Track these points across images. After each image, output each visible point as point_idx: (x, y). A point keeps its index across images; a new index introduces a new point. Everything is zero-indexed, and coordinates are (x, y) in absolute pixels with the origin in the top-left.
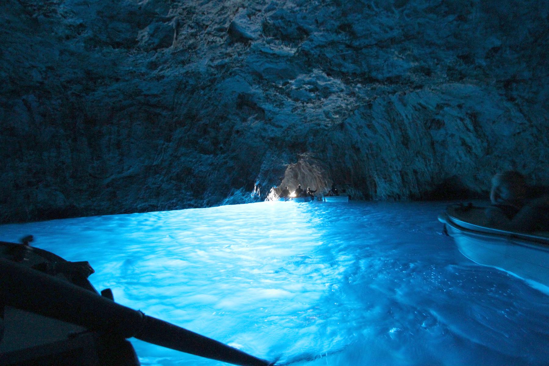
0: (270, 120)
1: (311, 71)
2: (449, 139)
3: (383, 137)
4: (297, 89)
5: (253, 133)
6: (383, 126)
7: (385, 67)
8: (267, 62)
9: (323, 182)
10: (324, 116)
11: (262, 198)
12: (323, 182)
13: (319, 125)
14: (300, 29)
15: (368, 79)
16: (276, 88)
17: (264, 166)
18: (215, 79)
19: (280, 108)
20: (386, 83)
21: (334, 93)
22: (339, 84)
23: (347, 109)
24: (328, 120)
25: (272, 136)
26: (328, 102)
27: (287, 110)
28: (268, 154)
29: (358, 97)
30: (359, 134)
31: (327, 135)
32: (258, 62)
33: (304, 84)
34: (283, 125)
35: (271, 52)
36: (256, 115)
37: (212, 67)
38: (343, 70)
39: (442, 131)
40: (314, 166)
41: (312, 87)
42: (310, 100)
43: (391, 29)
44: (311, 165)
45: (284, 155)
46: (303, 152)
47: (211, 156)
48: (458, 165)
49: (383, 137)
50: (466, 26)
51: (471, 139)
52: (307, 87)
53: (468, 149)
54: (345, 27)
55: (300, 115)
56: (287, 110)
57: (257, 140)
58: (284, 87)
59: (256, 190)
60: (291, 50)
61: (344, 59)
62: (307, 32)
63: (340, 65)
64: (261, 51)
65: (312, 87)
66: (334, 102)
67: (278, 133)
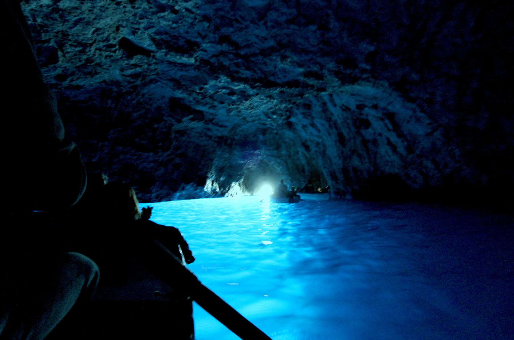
2: (378, 138)
5: (197, 133)
6: (323, 125)
8: (179, 70)
11: (222, 192)
13: (265, 125)
14: (188, 41)
18: (137, 86)
28: (219, 152)
31: (277, 134)
34: (227, 124)
36: (191, 116)
39: (370, 130)
43: (266, 39)
45: (235, 152)
46: (255, 149)
47: (151, 154)
48: (389, 164)
50: (331, 35)
51: (394, 138)
53: (394, 148)
54: (224, 39)
57: (204, 138)
62: (198, 45)
67: (225, 132)
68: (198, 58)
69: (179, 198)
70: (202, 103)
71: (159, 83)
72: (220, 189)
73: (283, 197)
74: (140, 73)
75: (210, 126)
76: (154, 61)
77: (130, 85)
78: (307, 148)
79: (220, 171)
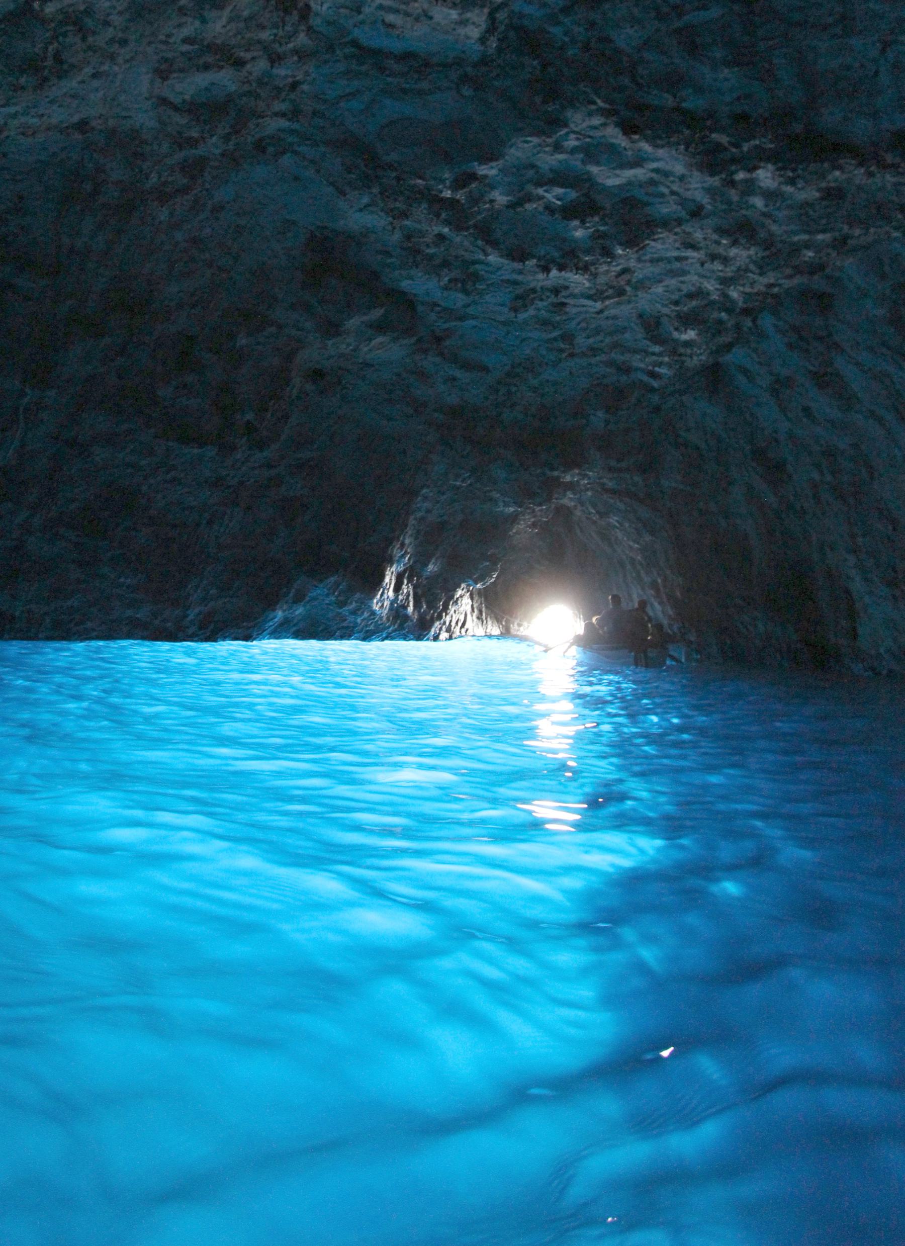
0: (439, 340)
1: (556, 122)
3: (880, 420)
4: (511, 206)
7: (884, 79)
9: (647, 579)
10: (640, 334)
11: (418, 622)
12: (647, 579)
15: (805, 146)
16: (436, 202)
17: (427, 506)
18: (201, 163)
19: (467, 293)
20: (889, 158)
21: (665, 223)
22: (682, 178)
23: (727, 305)
24: (657, 349)
25: (453, 399)
26: (650, 270)
27: (495, 302)
29: (768, 244)
30: (783, 410)
31: (657, 409)
32: (352, 95)
33: (539, 184)
35: (397, 46)
36: (377, 313)
37: (176, 109)
38: (693, 103)
40: (613, 520)
41: (573, 194)
42: (569, 257)
44: (602, 515)
46: (569, 465)
49: (880, 420)
52: (554, 195)
55: (545, 323)
56: (495, 302)
58: (461, 195)
59: (397, 589)
60: (463, 23)
61: (693, 49)
63: (673, 81)
64: (355, 43)
65: (573, 194)
66: (673, 273)
68: (501, 16)
69: (277, 634)
70: (431, 257)
71: (287, 160)
72: (417, 605)
73: (612, 649)
74: (230, 99)
75: (430, 362)
76: (302, 39)
77: (179, 156)
78: (776, 471)
79: (430, 540)
